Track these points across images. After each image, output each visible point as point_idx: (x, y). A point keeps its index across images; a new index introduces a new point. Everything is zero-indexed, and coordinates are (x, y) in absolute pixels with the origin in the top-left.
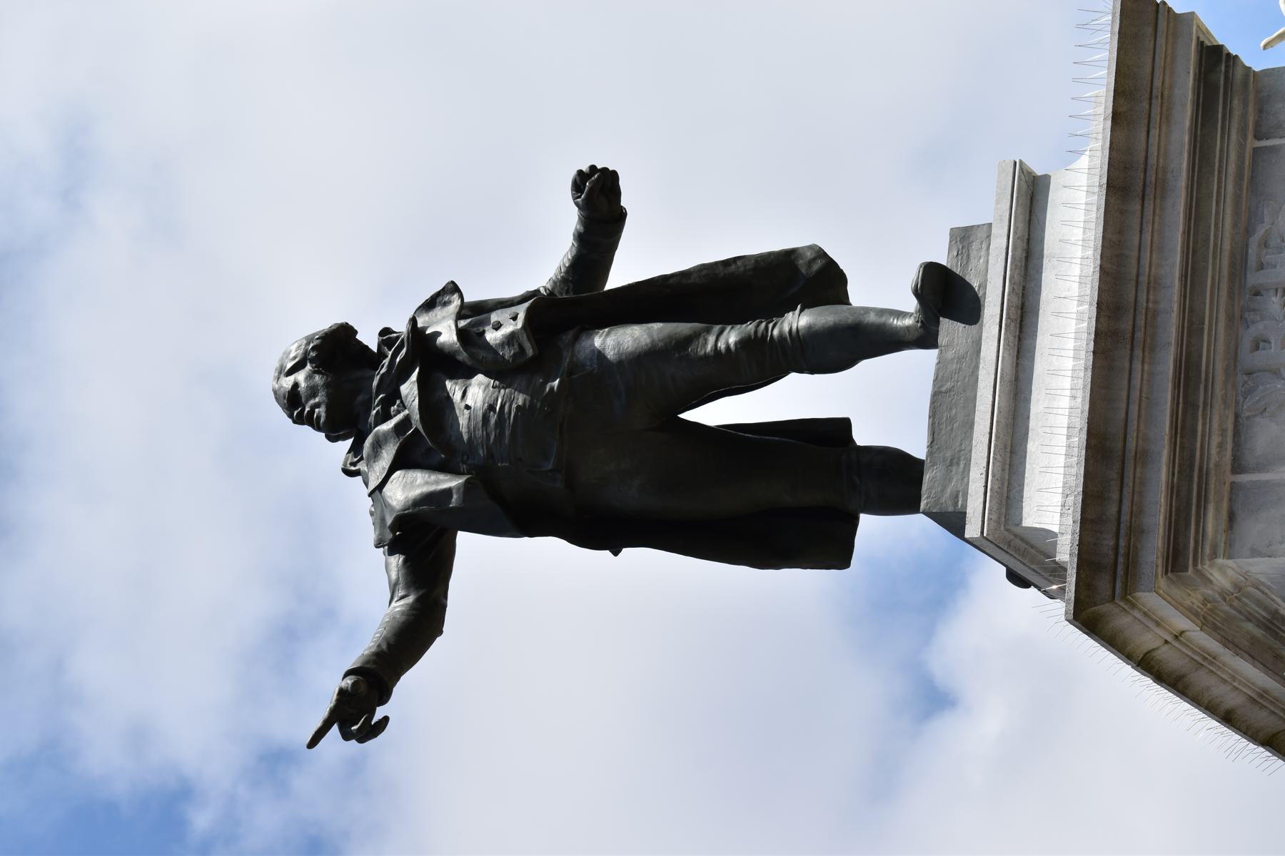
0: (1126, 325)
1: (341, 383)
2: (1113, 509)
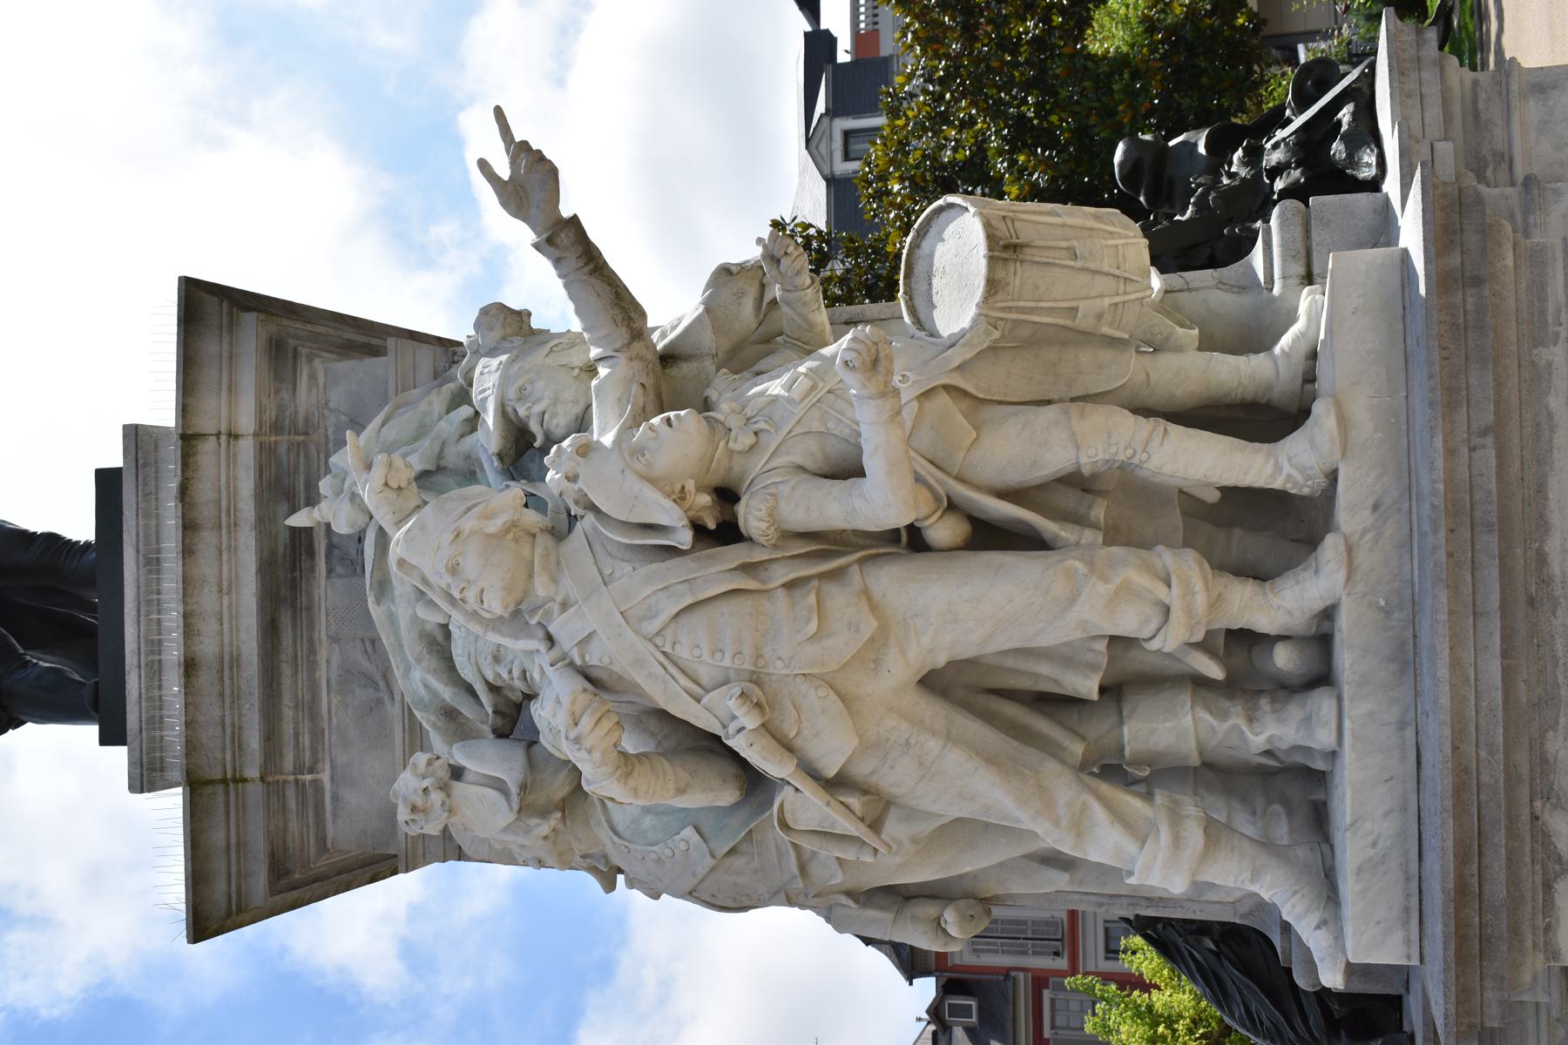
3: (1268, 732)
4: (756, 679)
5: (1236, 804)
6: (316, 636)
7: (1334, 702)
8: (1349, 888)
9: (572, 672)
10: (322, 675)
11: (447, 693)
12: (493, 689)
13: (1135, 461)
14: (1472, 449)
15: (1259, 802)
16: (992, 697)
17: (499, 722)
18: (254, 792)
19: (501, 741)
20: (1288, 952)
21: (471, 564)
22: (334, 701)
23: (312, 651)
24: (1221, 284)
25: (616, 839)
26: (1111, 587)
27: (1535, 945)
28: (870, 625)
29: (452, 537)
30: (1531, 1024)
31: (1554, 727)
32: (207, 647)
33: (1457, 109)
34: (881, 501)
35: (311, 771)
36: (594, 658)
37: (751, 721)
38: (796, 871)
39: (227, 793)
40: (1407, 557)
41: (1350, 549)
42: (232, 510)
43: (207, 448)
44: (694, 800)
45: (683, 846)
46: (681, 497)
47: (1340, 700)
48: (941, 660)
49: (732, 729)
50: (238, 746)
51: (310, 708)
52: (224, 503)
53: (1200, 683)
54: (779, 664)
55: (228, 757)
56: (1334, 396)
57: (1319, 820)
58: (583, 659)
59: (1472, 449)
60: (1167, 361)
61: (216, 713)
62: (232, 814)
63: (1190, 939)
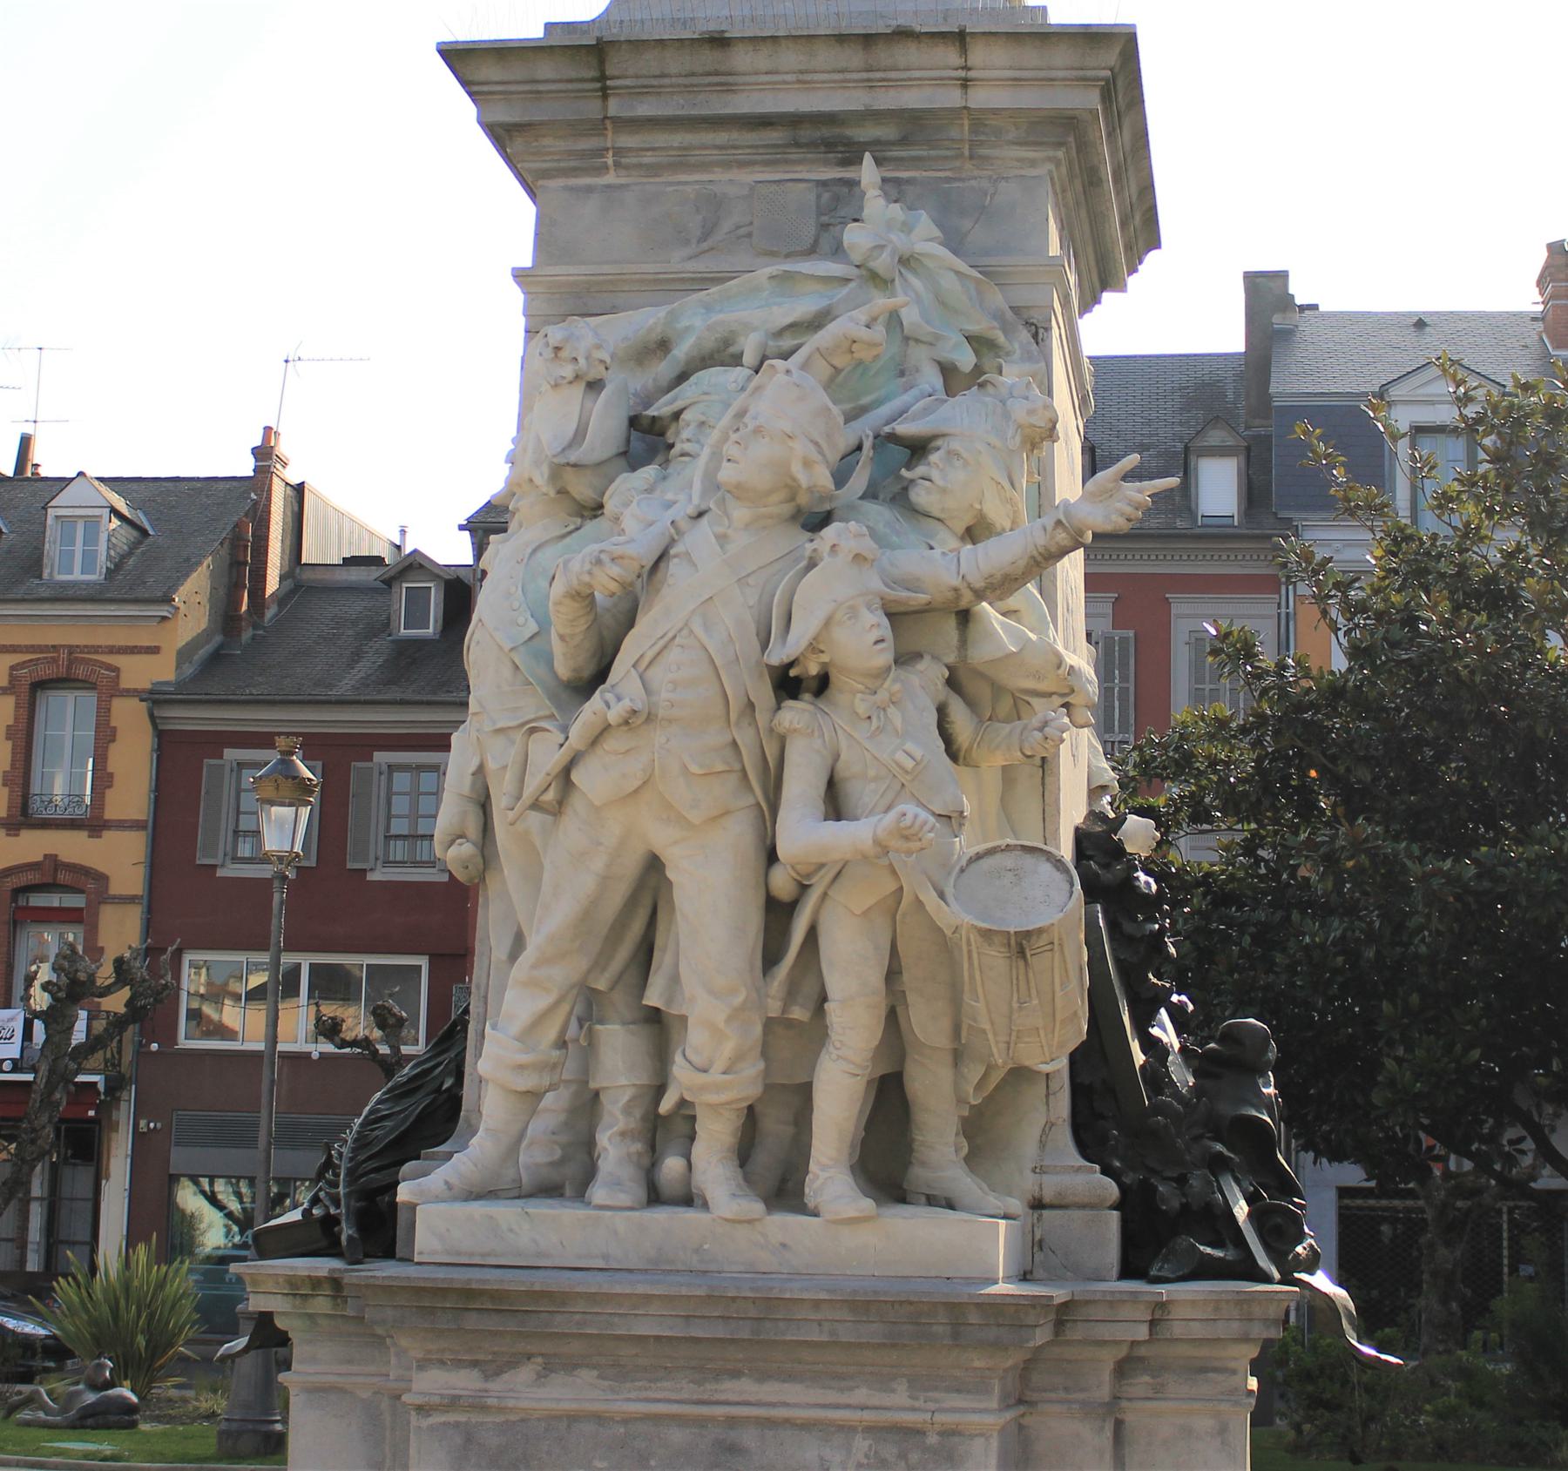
3: (615, 1150)
4: (650, 718)
5: (562, 1117)
6: (757, 168)
7: (629, 1204)
8: (478, 1209)
9: (666, 541)
10: (719, 175)
11: (682, 351)
12: (677, 416)
13: (831, 1049)
14: (820, 1323)
15: (563, 1138)
16: (642, 911)
17: (645, 422)
18: (592, 109)
19: (625, 423)
20: (432, 1157)
21: (762, 450)
22: (689, 189)
23: (742, 164)
24: (1050, 1125)
25: (529, 550)
26: (722, 1025)
27: (429, 1352)
28: (695, 817)
29: (788, 430)
30: (372, 1369)
31: (600, 1377)
32: (742, 59)
33: (1204, 1352)
34: (803, 832)
35: (617, 165)
36: (674, 567)
37: (613, 716)
38: (499, 725)
39: (593, 80)
40: (742, 1268)
41: (750, 1222)
42: (888, 84)
43: (951, 56)
44: (558, 648)
45: (521, 620)
46: (813, 648)
47: (631, 1209)
48: (670, 874)
49: (609, 696)
50: (642, 92)
51: (681, 163)
52: (893, 75)
53: (660, 1090)
54: (663, 740)
55: (627, 82)
56: (878, 1215)
57: (549, 1190)
58: (676, 556)
59: (820, 1323)
60: (945, 1074)
61: (673, 70)
62: (570, 86)
63: (452, 1066)
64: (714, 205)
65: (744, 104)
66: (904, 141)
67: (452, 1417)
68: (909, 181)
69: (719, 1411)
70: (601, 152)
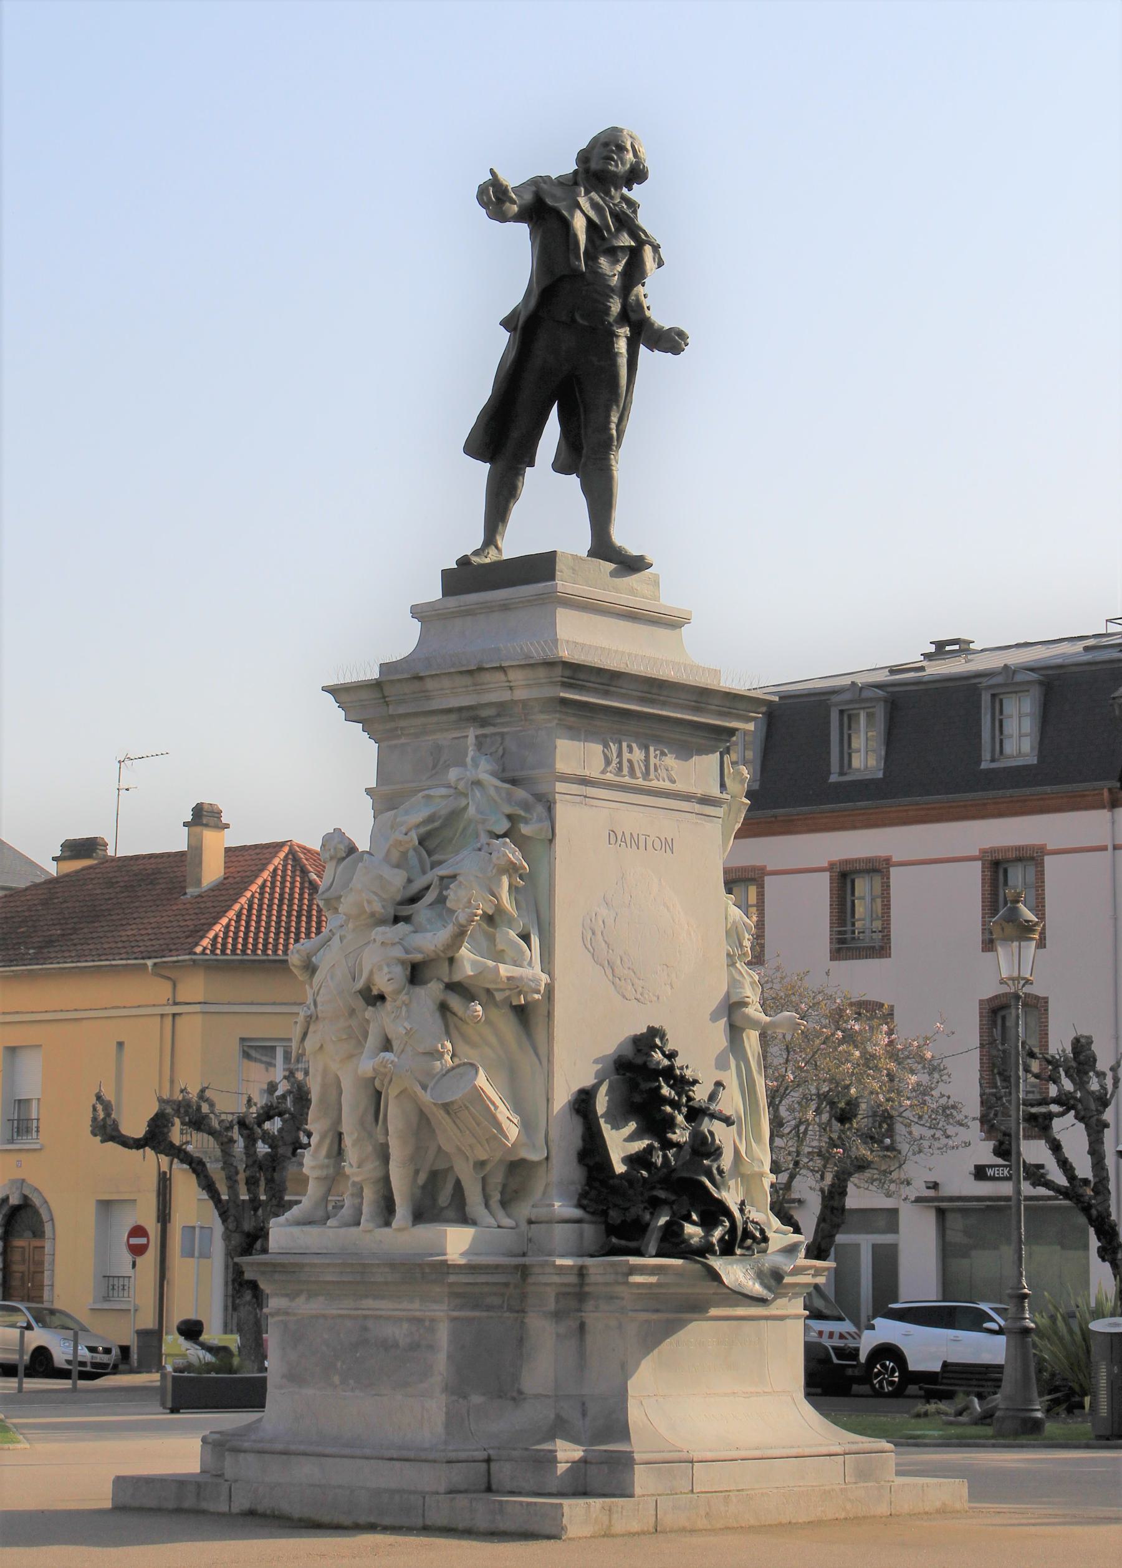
0: (655, 691)
1: (607, 166)
2: (592, 679)
23: (447, 730)
32: (430, 685)
64: (438, 749)
65: (436, 705)
66: (499, 715)
67: (280, 1318)
68: (507, 733)
69: (359, 1312)
70: (396, 729)
